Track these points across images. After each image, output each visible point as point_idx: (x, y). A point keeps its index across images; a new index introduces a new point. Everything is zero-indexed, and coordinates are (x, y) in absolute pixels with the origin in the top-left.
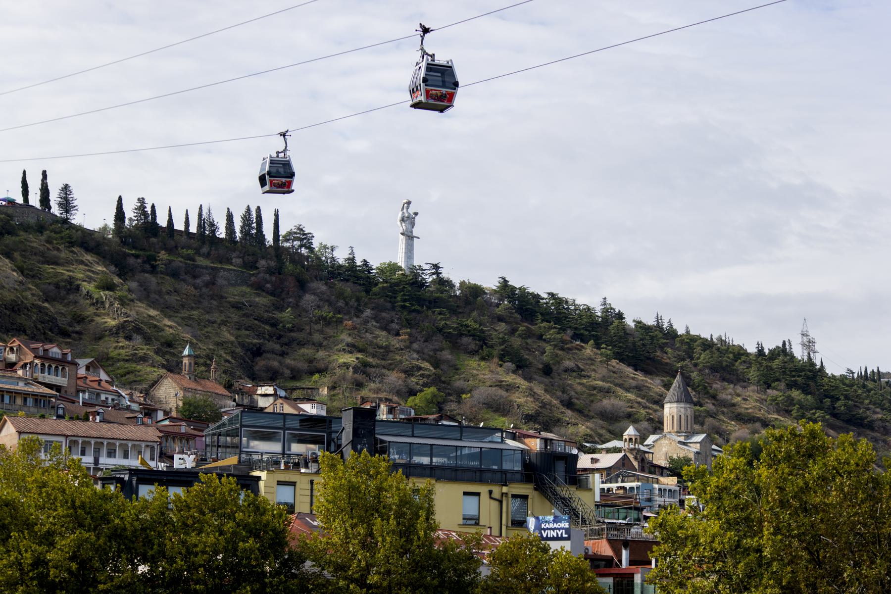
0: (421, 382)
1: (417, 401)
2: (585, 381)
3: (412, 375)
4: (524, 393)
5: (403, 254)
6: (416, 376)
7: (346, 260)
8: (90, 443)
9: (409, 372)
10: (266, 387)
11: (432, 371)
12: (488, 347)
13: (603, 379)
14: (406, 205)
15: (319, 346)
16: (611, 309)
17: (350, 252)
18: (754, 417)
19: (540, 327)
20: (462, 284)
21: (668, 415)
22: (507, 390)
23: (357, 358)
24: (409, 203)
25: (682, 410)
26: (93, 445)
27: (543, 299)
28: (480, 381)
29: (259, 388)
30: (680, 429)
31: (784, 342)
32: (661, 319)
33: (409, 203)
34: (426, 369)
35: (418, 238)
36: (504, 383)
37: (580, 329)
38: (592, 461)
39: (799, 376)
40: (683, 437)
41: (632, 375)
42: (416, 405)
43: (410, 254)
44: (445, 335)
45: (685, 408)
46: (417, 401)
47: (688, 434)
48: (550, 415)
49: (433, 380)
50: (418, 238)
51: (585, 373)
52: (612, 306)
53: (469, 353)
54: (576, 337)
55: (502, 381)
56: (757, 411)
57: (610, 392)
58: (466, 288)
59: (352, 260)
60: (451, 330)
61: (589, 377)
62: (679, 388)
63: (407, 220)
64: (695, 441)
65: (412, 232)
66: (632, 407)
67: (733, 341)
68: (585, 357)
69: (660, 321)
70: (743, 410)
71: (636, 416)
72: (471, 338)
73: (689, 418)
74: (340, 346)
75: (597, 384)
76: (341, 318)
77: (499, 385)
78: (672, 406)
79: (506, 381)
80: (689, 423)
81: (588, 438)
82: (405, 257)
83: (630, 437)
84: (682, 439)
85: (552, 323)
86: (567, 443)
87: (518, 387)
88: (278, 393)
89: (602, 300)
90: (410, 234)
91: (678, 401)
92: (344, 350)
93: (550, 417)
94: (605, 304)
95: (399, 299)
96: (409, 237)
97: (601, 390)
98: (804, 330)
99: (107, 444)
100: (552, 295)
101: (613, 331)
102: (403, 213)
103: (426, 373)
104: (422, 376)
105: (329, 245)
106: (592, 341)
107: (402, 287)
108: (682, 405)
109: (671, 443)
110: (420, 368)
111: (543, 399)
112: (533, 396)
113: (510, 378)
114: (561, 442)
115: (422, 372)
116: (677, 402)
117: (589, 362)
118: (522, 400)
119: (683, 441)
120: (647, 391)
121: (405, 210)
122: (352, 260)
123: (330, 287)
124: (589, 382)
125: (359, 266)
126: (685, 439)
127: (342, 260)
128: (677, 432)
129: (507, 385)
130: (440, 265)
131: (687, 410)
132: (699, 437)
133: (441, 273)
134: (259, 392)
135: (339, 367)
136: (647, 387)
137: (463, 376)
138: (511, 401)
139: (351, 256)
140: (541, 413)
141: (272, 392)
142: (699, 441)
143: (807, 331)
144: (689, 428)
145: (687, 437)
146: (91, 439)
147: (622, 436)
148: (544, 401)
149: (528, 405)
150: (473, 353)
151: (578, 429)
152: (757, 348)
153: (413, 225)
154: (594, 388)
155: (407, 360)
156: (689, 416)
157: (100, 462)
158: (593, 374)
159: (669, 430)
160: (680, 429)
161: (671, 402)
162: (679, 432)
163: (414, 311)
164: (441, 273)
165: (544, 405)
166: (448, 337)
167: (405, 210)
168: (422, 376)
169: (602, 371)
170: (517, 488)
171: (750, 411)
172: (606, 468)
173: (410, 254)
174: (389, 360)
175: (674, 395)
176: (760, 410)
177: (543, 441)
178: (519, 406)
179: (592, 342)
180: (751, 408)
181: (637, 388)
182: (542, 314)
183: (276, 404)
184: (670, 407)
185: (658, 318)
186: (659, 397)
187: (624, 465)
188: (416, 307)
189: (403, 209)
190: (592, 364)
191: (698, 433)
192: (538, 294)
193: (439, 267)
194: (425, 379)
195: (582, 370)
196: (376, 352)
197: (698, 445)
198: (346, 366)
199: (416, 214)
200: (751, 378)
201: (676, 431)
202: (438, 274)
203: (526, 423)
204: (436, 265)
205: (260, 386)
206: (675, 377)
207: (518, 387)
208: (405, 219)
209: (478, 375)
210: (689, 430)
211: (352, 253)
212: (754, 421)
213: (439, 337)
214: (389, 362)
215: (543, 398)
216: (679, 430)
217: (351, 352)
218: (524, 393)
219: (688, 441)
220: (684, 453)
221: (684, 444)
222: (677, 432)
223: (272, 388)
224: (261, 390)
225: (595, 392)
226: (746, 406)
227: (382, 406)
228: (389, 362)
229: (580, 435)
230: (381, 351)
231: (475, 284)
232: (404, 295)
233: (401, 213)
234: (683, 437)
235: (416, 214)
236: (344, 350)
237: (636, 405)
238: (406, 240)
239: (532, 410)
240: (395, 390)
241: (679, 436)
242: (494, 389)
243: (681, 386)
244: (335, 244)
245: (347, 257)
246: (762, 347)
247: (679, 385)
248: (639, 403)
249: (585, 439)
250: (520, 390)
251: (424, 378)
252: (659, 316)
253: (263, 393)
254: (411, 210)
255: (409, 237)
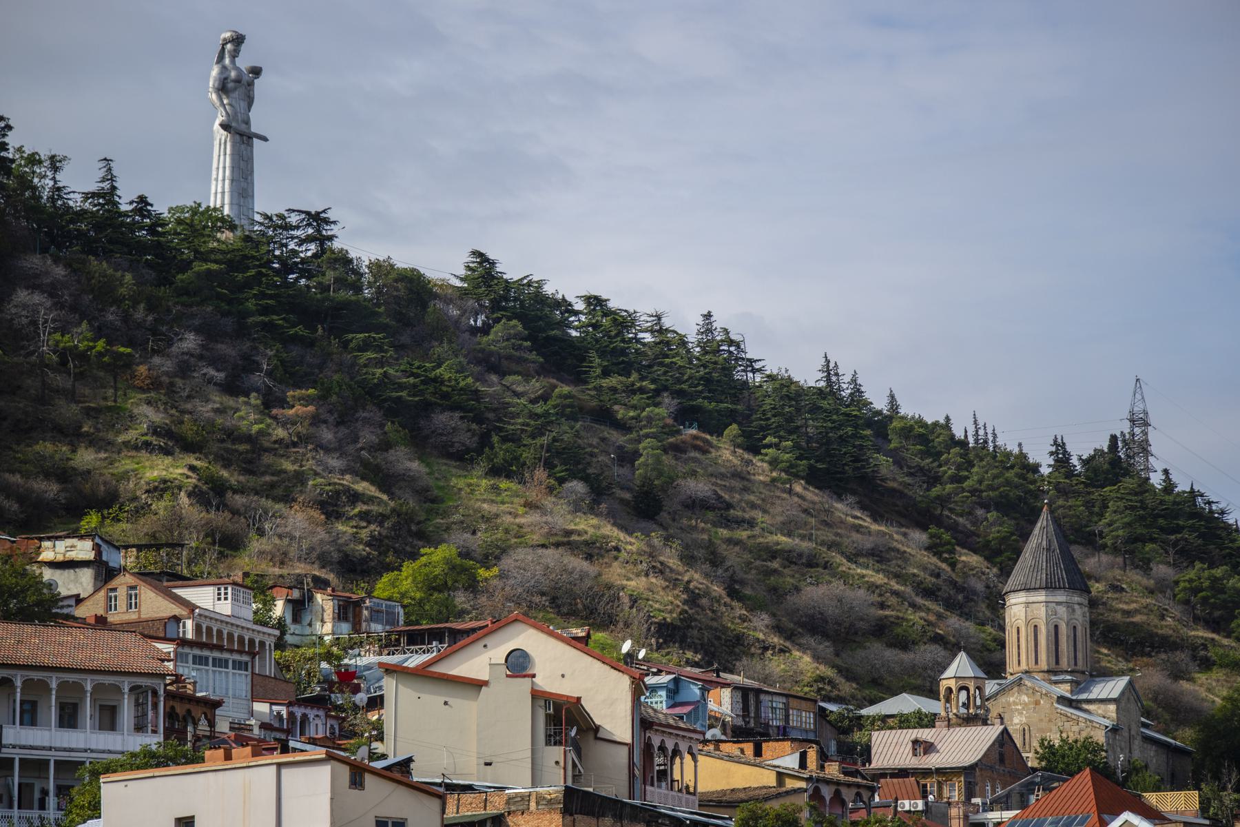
0: (364, 534)
1: (406, 585)
2: (743, 534)
3: (339, 516)
4: (635, 564)
5: (227, 182)
6: (350, 518)
7: (87, 196)
8: (44, 686)
9: (331, 506)
10: (69, 542)
11: (386, 504)
12: (505, 440)
13: (788, 528)
14: (229, 46)
15: (72, 435)
16: (731, 342)
17: (102, 173)
18: (1152, 635)
19: (599, 389)
20: (379, 268)
21: (1021, 624)
22: (589, 557)
23: (192, 468)
24: (238, 40)
25: (1062, 610)
26: (54, 692)
27: (576, 313)
28: (507, 531)
29: (46, 544)
30: (1057, 662)
31: (1114, 439)
32: (837, 374)
33: (238, 40)
34: (371, 500)
35: (265, 139)
36: (574, 538)
37: (692, 397)
38: (914, 750)
39: (1117, 529)
40: (1067, 687)
41: (850, 519)
42: (403, 595)
43: (243, 184)
44: (386, 405)
45: (1068, 605)
46: (406, 585)
47: (1079, 677)
48: (715, 624)
49: (393, 528)
50: (265, 139)
51: (740, 513)
52: (733, 337)
53: (450, 456)
54: (685, 415)
55: (569, 533)
56: (1156, 621)
57: (817, 565)
58: (396, 281)
59: (108, 195)
60: (404, 394)
61: (751, 524)
62: (1048, 550)
63: (235, 89)
64: (1103, 696)
65: (247, 122)
66: (882, 606)
67: (995, 436)
68: (723, 470)
69: (834, 379)
70: (1119, 616)
71: (899, 630)
72: (457, 415)
73: (1079, 633)
74: (131, 435)
75: (778, 543)
76: (129, 355)
77: (565, 541)
78: (1032, 599)
79: (579, 533)
80: (1079, 646)
81: (828, 688)
82: (232, 192)
83: (961, 683)
84: (1064, 690)
85: (634, 376)
86: (793, 702)
87: (617, 549)
88: (104, 558)
89: (700, 320)
90: (243, 127)
91: (1049, 587)
92: (147, 445)
93: (716, 629)
94: (709, 330)
95: (251, 305)
96: (241, 135)
97: (790, 558)
98: (1136, 409)
99: (25, 683)
100: (595, 302)
101: (768, 401)
102: (224, 68)
103: (375, 508)
104: (364, 516)
105: (44, 154)
106: (734, 426)
107: (252, 272)
108: (1061, 597)
109: (1037, 703)
110: (355, 497)
111: (689, 582)
112: (661, 572)
113: (588, 525)
114: (776, 698)
115: (360, 507)
116: (1046, 588)
117: (737, 484)
118: (637, 584)
119: (1068, 695)
120: (899, 562)
121: (227, 61)
122: (108, 195)
123: (74, 271)
124: (754, 536)
125: (125, 214)
126: (1072, 692)
127: (78, 197)
128: (1048, 672)
129: (586, 543)
130: (331, 215)
131: (1074, 610)
132: (1111, 684)
133: (331, 238)
134: (47, 555)
135: (147, 491)
136: (898, 551)
137: (457, 517)
138: (609, 587)
139: (106, 185)
140: (691, 619)
141: (91, 556)
142: (1115, 695)
143: (1146, 413)
144: (1080, 662)
145: (1077, 686)
146: (83, 676)
147: (936, 682)
148: (691, 586)
149: (658, 597)
150: (464, 458)
151: (794, 662)
152: (1052, 453)
153: (250, 101)
154: (773, 553)
155: (316, 474)
156: (1079, 628)
157: (4, 742)
158: (758, 515)
159: (1024, 667)
160: (1057, 662)
161: (1028, 590)
162: (1055, 673)
163: (295, 339)
164: (331, 238)
165: (693, 598)
166: (394, 410)
167: (227, 61)
168: (364, 516)
169: (784, 508)
170: (49, 803)
171: (1137, 619)
172: (965, 768)
173: (243, 184)
174: (263, 474)
175: (1035, 568)
176: (1162, 617)
177: (739, 694)
178: (634, 601)
179: (733, 429)
180: (1137, 611)
181: (873, 555)
182: (602, 354)
183: (114, 590)
184: (1027, 604)
185: (828, 371)
186: (934, 580)
187: (1002, 760)
188: (299, 330)
189: (221, 58)
190: (745, 490)
191: (1106, 674)
192: (564, 299)
193: (327, 221)
194: (372, 527)
195: (729, 506)
196: (227, 450)
197: (1112, 707)
198: (162, 488)
199: (256, 72)
200: (1106, 530)
201: (1045, 668)
202: (322, 240)
203: (659, 647)
204: (318, 213)
205: (49, 539)
206: (1033, 520)
207: (617, 549)
208: (230, 85)
209: (497, 516)
210: (1080, 666)
211: (110, 177)
212: (1152, 646)
213: (371, 412)
214: (268, 478)
215: (686, 578)
216: (1053, 665)
217: (167, 452)
218: (635, 564)
219: (1084, 696)
220: (1076, 728)
221: (1069, 703)
222: (1048, 672)
223: (88, 544)
224: (51, 551)
225: (775, 565)
226: (1125, 607)
227: (319, 597)
228: (268, 478)
229: (807, 679)
230: (242, 447)
231: (413, 270)
232: (263, 295)
233: (215, 71)
234: (1067, 687)
235: (256, 72)
236: (147, 445)
237: (893, 600)
238: (233, 146)
239: (671, 612)
240: (314, 555)
241: (1056, 683)
242: (550, 552)
243: (1055, 544)
244: (59, 152)
245: (93, 187)
246: (1065, 452)
247: (1049, 542)
248: (896, 593)
249: (819, 690)
250: (623, 555)
251: (369, 522)
252: (832, 365)
253: (60, 558)
254: (244, 62)
255: (241, 135)
